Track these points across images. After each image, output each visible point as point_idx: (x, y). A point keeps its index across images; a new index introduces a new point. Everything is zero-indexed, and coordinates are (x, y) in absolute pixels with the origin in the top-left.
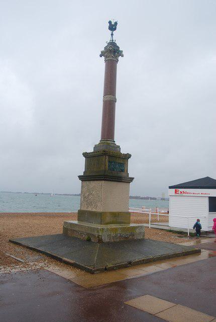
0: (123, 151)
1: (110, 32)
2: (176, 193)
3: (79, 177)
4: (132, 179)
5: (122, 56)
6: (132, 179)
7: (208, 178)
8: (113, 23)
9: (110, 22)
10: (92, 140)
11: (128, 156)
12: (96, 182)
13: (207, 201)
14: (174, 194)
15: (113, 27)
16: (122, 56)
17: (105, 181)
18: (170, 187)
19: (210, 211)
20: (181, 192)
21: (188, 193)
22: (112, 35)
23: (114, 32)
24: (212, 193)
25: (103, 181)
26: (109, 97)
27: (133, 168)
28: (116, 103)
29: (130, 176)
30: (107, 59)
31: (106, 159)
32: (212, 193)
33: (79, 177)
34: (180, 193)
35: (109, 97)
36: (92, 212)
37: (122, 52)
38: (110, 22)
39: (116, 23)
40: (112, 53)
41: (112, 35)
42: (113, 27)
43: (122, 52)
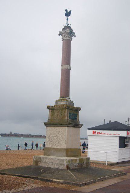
0: (76, 105)
1: (66, 17)
2: (93, 133)
3: (45, 123)
4: (82, 125)
5: (75, 36)
6: (82, 125)
7: (116, 122)
8: (68, 12)
9: (66, 11)
10: (53, 96)
11: (79, 109)
12: (59, 127)
13: (117, 140)
14: (92, 134)
15: (68, 14)
16: (75, 36)
17: (68, 127)
18: (89, 129)
19: (120, 147)
20: (98, 133)
21: (103, 134)
22: (67, 20)
23: (69, 17)
24: (124, 134)
25: (67, 127)
26: (66, 67)
27: (82, 116)
28: (71, 70)
29: (80, 123)
30: (64, 38)
31: (65, 112)
32: (124, 134)
33: (45, 123)
34: (97, 133)
35: (66, 67)
36: (58, 149)
37: (75, 33)
38: (66, 11)
39: (70, 12)
40: (68, 34)
41: (67, 20)
42: (68, 14)
43: (75, 33)
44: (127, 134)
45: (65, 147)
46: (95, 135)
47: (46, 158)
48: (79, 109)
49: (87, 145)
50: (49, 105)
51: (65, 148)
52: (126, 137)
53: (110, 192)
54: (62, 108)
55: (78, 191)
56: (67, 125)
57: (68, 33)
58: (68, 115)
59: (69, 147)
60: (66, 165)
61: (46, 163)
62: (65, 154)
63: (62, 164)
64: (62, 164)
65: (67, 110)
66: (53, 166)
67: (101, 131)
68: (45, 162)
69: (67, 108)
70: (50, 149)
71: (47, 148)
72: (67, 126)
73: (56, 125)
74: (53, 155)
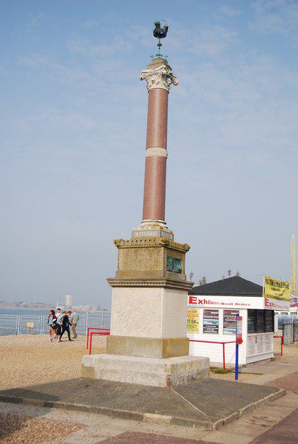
0: (179, 240)
1: (156, 40)
8: (162, 27)
9: (158, 25)
11: (183, 250)
19: (248, 333)
20: (200, 302)
21: (212, 303)
26: (157, 152)
34: (198, 302)
38: (158, 25)
44: (266, 302)
45: (160, 336)
46: (194, 305)
47: (134, 364)
48: (183, 250)
49: (64, 314)
50: (118, 239)
51: (158, 337)
52: (265, 310)
53: (282, 443)
54: (149, 245)
55: (190, 440)
56: (164, 285)
57: (163, 75)
58: (164, 259)
59: (167, 337)
60: (164, 377)
61: (115, 372)
62: (159, 351)
63: (154, 376)
64: (154, 376)
65: (162, 248)
66: (132, 379)
67: (207, 298)
68: (110, 371)
69: (162, 246)
70: (123, 339)
71: (114, 337)
72: (165, 287)
73: (138, 284)
74: (129, 354)
